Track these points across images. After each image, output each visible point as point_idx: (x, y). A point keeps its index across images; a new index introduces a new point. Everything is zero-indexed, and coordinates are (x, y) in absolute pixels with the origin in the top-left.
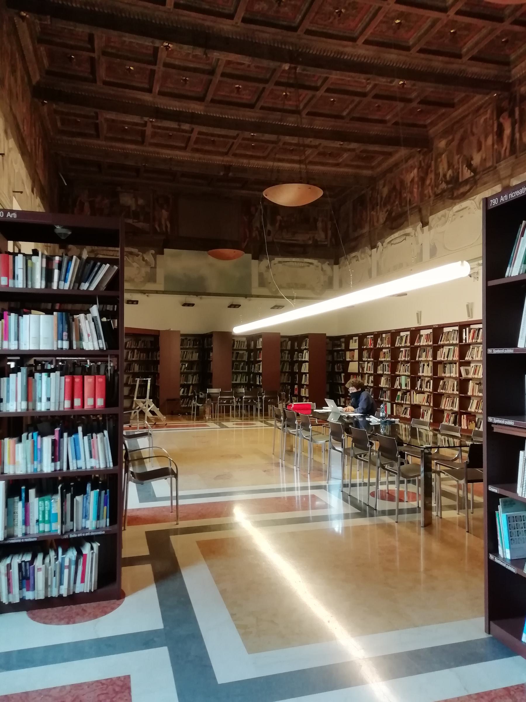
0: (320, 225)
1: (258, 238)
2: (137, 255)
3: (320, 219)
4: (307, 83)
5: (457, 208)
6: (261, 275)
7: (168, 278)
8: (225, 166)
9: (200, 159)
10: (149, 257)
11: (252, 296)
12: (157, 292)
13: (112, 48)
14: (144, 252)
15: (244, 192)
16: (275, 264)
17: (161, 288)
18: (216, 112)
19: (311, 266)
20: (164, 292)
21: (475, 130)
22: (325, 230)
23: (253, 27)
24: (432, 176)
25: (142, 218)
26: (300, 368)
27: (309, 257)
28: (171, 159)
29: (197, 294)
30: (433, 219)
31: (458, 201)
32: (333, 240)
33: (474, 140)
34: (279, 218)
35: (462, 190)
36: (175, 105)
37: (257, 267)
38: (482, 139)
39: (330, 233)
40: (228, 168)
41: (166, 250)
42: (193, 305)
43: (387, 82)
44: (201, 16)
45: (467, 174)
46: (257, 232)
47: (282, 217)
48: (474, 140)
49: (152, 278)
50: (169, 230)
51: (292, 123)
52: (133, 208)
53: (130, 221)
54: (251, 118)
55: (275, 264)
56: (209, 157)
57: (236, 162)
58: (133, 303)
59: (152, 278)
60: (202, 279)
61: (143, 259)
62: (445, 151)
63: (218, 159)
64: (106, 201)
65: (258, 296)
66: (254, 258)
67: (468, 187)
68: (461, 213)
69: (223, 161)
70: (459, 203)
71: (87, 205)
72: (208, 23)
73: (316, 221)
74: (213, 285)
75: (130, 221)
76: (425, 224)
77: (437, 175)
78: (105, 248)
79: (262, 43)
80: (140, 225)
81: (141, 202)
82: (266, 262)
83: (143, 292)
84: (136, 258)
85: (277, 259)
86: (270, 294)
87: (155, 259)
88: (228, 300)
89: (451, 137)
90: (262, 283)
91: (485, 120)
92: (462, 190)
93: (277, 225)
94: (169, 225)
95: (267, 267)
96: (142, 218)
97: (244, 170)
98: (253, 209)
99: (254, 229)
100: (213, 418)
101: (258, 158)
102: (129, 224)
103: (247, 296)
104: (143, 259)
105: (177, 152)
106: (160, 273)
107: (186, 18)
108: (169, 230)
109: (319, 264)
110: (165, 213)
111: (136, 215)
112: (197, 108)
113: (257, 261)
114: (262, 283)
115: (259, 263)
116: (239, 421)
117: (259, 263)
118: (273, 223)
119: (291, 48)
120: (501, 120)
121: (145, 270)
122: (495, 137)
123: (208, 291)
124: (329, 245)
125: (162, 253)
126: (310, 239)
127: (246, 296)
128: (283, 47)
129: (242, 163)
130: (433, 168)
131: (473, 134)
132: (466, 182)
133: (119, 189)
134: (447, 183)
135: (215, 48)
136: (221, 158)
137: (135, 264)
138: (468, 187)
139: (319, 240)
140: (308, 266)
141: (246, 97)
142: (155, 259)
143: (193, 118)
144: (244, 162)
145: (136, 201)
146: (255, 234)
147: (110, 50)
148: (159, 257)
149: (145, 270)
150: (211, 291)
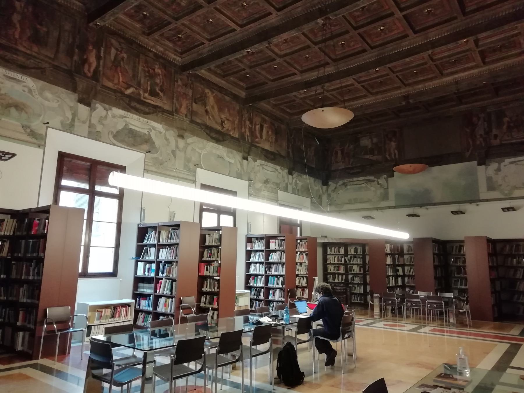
1: (483, 145)
2: (374, 181)
4: (384, 14)
6: (489, 179)
7: (398, 196)
8: (404, 96)
9: (382, 98)
10: (382, 181)
11: (481, 201)
12: (390, 208)
13: (254, 62)
14: (378, 178)
15: (463, 107)
16: (505, 166)
17: (393, 204)
18: (343, 66)
20: (395, 207)
23: (286, 10)
25: (376, 152)
26: (515, 273)
28: (362, 106)
29: (421, 206)
34: (506, 120)
36: (313, 75)
37: (483, 173)
40: (406, 97)
42: (418, 216)
44: (257, 23)
46: (481, 139)
49: (385, 197)
50: (397, 156)
51: (408, 46)
52: (370, 146)
53: (367, 157)
54: (370, 59)
55: (505, 166)
56: (389, 94)
57: (410, 90)
58: (509, 211)
59: (385, 197)
60: (427, 191)
61: (378, 184)
63: (398, 93)
64: (352, 147)
65: (487, 200)
66: (479, 164)
69: (401, 93)
71: (339, 153)
72: (263, 24)
74: (438, 195)
75: (367, 157)
78: (351, 180)
79: (299, 16)
80: (374, 158)
81: (375, 140)
82: (494, 166)
83: (377, 209)
84: (373, 183)
85: (507, 161)
86: (503, 197)
87: (387, 181)
88: (454, 207)
90: (491, 187)
93: (505, 127)
94: (396, 152)
96: (376, 152)
97: (421, 93)
98: (475, 119)
99: (478, 137)
100: (383, 315)
101: (431, 79)
102: (368, 159)
103: (475, 200)
104: (378, 184)
105: (364, 100)
106: (392, 192)
107: (251, 30)
108: (397, 156)
110: (393, 144)
111: (371, 151)
112: (330, 70)
113: (483, 167)
114: (491, 187)
115: (486, 169)
116: (394, 321)
117: (486, 169)
119: (320, 6)
121: (380, 191)
123: (433, 202)
127: (471, 202)
128: (314, 9)
129: (419, 89)
133: (360, 135)
135: (273, 36)
136: (399, 92)
137: (372, 189)
141: (359, 46)
142: (387, 181)
143: (330, 78)
144: (420, 86)
145: (372, 141)
146: (479, 141)
147: (253, 64)
148: (390, 179)
149: (380, 191)
150: (437, 201)
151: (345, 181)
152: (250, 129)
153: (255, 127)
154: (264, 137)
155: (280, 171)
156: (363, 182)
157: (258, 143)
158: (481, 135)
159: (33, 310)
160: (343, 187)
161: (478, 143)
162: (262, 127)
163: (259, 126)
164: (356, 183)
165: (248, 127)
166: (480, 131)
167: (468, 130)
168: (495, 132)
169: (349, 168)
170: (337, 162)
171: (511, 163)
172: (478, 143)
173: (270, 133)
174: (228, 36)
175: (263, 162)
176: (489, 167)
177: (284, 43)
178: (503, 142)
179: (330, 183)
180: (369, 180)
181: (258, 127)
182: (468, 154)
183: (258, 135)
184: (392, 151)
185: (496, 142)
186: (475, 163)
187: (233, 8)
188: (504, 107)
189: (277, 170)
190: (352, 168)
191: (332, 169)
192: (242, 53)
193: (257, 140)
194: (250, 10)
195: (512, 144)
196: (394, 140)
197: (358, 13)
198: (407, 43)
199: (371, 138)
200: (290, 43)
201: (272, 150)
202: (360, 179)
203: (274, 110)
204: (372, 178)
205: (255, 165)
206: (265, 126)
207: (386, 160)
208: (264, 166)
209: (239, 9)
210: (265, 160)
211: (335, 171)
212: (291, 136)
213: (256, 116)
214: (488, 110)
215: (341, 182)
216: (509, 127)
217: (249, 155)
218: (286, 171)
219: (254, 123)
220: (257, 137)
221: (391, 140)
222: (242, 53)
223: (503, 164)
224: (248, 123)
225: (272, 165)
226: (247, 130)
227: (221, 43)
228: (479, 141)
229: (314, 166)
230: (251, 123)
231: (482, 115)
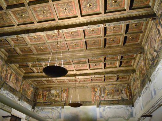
0: (123, 92)
3: (123, 89)
5: (156, 70)
14: (57, 108)
19: (122, 108)
21: (153, 37)
22: (126, 93)
24: (147, 61)
27: (120, 105)
30: (152, 78)
31: (156, 67)
32: (130, 97)
33: (153, 40)
34: (106, 91)
35: (156, 61)
38: (155, 39)
39: (128, 94)
41: (65, 107)
43: (97, 27)
45: (155, 54)
46: (98, 97)
47: (108, 91)
48: (153, 40)
50: (66, 100)
53: (54, 98)
61: (57, 111)
62: (148, 49)
64: (47, 93)
67: (157, 60)
68: (158, 72)
70: (156, 67)
71: (42, 94)
73: (121, 90)
75: (54, 98)
76: (150, 81)
77: (148, 60)
78: (45, 107)
80: (57, 99)
81: (58, 92)
89: (148, 44)
91: (154, 31)
92: (156, 61)
93: (106, 94)
94: (66, 98)
95: (103, 110)
96: (57, 97)
107: (22, 28)
108: (66, 100)
109: (126, 107)
110: (65, 94)
117: (100, 109)
118: (104, 93)
120: (158, 28)
122: (158, 35)
124: (129, 99)
125: (64, 108)
126: (120, 97)
130: (147, 58)
131: (152, 38)
132: (156, 57)
133: (51, 89)
134: (151, 61)
138: (157, 60)
139: (124, 97)
140: (121, 108)
148: (62, 109)
151: (42, 108)
152: (6, 75)
153: (8, 74)
154: (11, 80)
155: (15, 98)
156: (50, 109)
157: (7, 82)
158: (98, 96)
159: (46, 28)
160: (41, 110)
161: (97, 98)
162: (11, 75)
163: (10, 75)
164: (47, 109)
165: (4, 73)
166: (98, 94)
167: (94, 93)
168: (103, 95)
169: (45, 102)
170: (40, 99)
171: (108, 108)
172: (97, 98)
173: (14, 79)
174: (9, 28)
175: (8, 92)
176: (100, 108)
177: (34, 39)
178: (106, 100)
179: (35, 108)
180: (53, 109)
181: (9, 75)
182: (93, 102)
183: (9, 79)
184: (64, 97)
185: (103, 99)
186: (96, 106)
187: (17, 15)
188: (106, 87)
189: (14, 97)
190: (46, 102)
191: (37, 102)
192: (14, 37)
193: (8, 81)
194: (24, 19)
195: (108, 101)
196: (65, 92)
197: (68, 35)
198: (83, 52)
199: (56, 90)
200: (36, 40)
201: (13, 88)
202: (49, 107)
203: (18, 69)
204: (54, 108)
205: (4, 93)
206: (13, 75)
207: (62, 101)
208: (8, 94)
209: (20, 17)
210: (9, 92)
211: (38, 102)
212: (23, 83)
213: (10, 69)
214: (101, 87)
215: (40, 108)
216: (107, 94)
217: (2, 87)
218: (18, 99)
219: (8, 72)
220: (7, 79)
221: (64, 92)
222: (14, 37)
223: (105, 108)
224: (5, 72)
225: (12, 94)
226: (4, 75)
227: (5, 30)
228: (97, 98)
229: (30, 99)
230: (7, 72)
231: (99, 88)
